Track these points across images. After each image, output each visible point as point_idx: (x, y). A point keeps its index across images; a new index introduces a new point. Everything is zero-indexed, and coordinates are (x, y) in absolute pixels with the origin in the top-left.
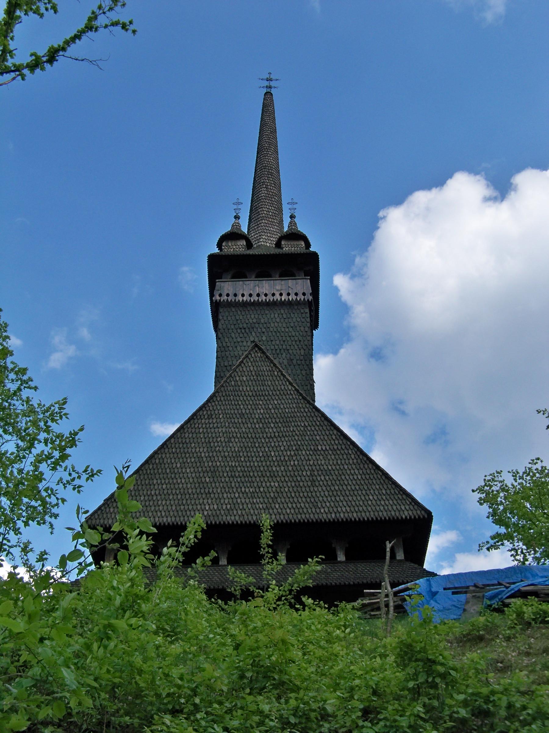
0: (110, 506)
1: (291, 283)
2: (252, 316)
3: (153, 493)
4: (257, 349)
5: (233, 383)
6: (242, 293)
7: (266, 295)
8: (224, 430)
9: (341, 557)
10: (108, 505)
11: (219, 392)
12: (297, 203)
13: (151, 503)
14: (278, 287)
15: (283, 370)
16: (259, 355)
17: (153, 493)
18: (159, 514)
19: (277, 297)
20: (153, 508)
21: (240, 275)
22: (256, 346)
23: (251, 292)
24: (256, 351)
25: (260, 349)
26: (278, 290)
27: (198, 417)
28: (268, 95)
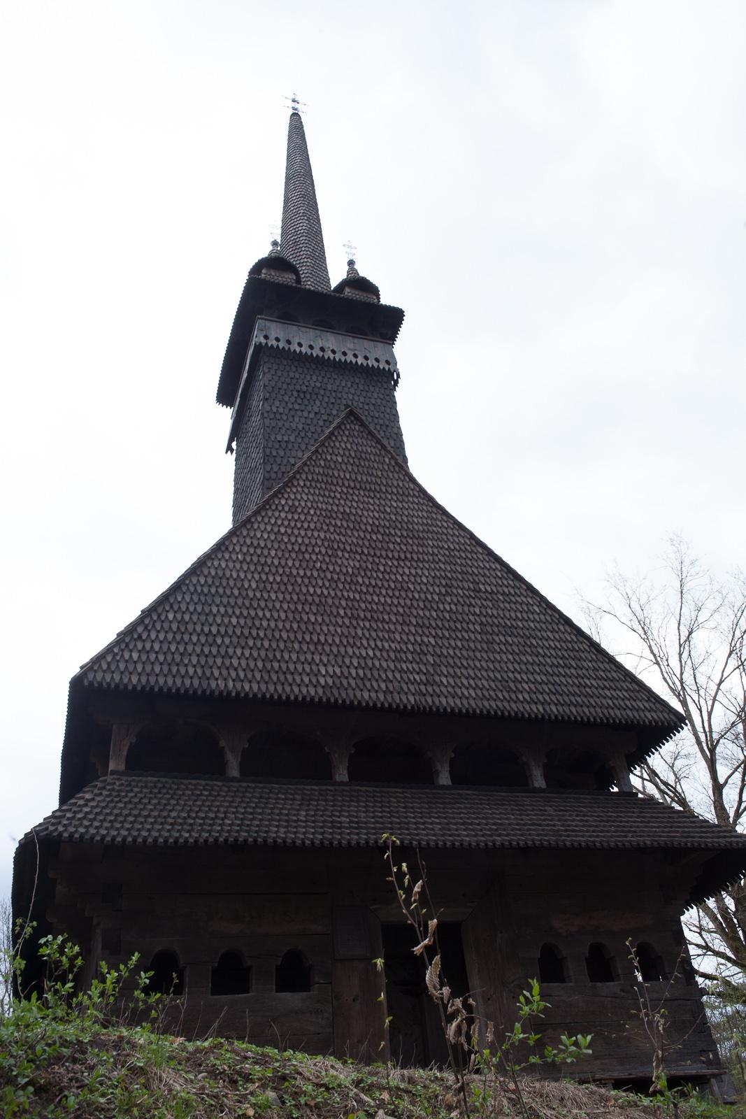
0: (131, 647)
1: (366, 343)
2: (313, 380)
3: (214, 630)
4: (353, 419)
5: (322, 463)
6: (298, 341)
7: (334, 352)
8: (322, 535)
9: (234, 772)
10: (127, 646)
11: (301, 473)
12: (355, 248)
13: (214, 651)
14: (352, 346)
15: (397, 457)
16: (357, 428)
17: (214, 630)
18: (233, 674)
19: (350, 358)
20: (219, 661)
21: (287, 317)
22: (351, 413)
23: (312, 343)
24: (352, 422)
25: (358, 419)
26: (350, 349)
27: (274, 507)
28: (296, 117)
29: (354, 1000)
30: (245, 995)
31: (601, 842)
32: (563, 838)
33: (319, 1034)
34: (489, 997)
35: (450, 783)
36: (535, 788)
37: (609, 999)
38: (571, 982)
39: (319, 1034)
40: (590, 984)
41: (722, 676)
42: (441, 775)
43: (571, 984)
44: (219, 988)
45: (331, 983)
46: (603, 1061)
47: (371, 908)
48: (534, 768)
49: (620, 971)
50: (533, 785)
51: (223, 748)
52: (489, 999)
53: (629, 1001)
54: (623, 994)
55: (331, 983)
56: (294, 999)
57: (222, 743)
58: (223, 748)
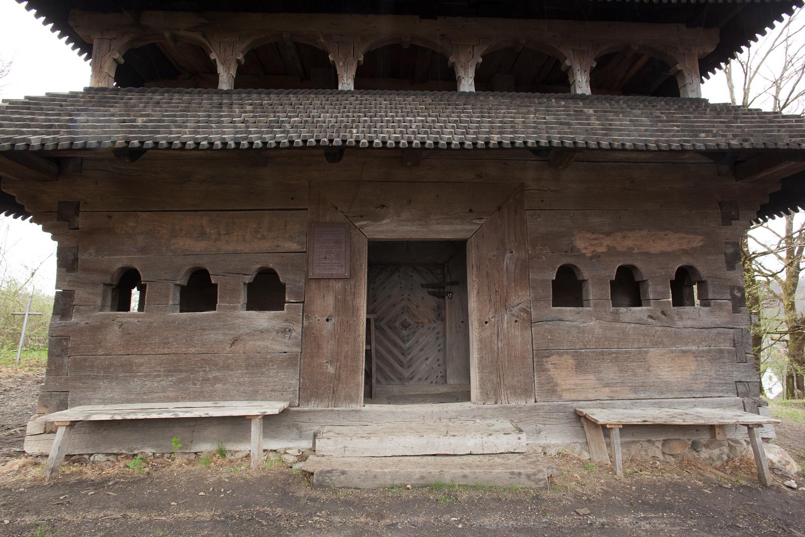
9: (225, 82)
29: (327, 320)
30: (212, 312)
31: (656, 142)
32: (482, 471)
33: (286, 353)
34: (487, 320)
35: (473, 90)
36: (578, 94)
37: (633, 325)
38: (589, 306)
39: (286, 353)
40: (612, 309)
41: (773, 45)
42: (463, 81)
43: (588, 308)
44: (255, 304)
45: (303, 302)
46: (613, 389)
47: (356, 224)
48: (579, 73)
49: (651, 297)
50: (575, 91)
51: (215, 60)
52: (486, 323)
53: (657, 328)
54: (650, 320)
55: (303, 302)
56: (263, 319)
57: (213, 56)
58: (215, 60)
